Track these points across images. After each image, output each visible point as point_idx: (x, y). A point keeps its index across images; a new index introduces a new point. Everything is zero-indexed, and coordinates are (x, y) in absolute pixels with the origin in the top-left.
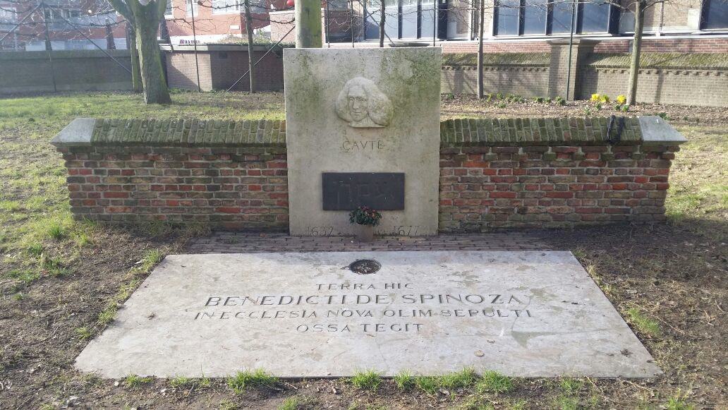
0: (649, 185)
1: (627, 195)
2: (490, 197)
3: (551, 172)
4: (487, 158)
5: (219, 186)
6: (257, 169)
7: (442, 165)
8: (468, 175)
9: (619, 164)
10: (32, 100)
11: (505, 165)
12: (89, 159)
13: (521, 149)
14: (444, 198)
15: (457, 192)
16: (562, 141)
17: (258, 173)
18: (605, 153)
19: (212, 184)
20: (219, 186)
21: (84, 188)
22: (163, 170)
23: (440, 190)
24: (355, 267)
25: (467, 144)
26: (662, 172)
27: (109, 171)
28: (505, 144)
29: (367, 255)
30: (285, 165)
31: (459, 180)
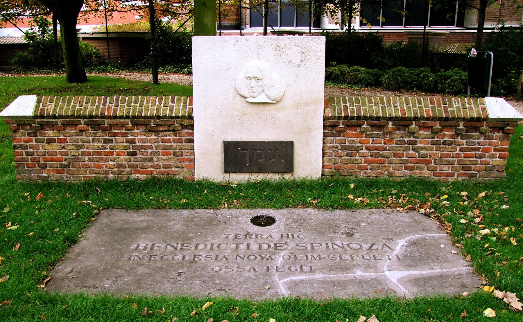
0: (492, 154)
1: (475, 162)
2: (365, 162)
3: (415, 143)
4: (362, 130)
5: (136, 152)
6: (168, 138)
7: (325, 135)
8: (347, 144)
9: (469, 137)
10: (10, 76)
11: (377, 136)
12: (31, 130)
13: (390, 123)
14: (326, 164)
15: (337, 158)
16: (423, 117)
17: (169, 141)
18: (459, 128)
19: (131, 150)
20: (136, 152)
21: (27, 153)
22: (91, 138)
23: (323, 157)
24: (257, 221)
25: (346, 117)
26: (503, 143)
27: (47, 139)
28: (378, 118)
29: (264, 212)
30: (192, 134)
31: (340, 147)
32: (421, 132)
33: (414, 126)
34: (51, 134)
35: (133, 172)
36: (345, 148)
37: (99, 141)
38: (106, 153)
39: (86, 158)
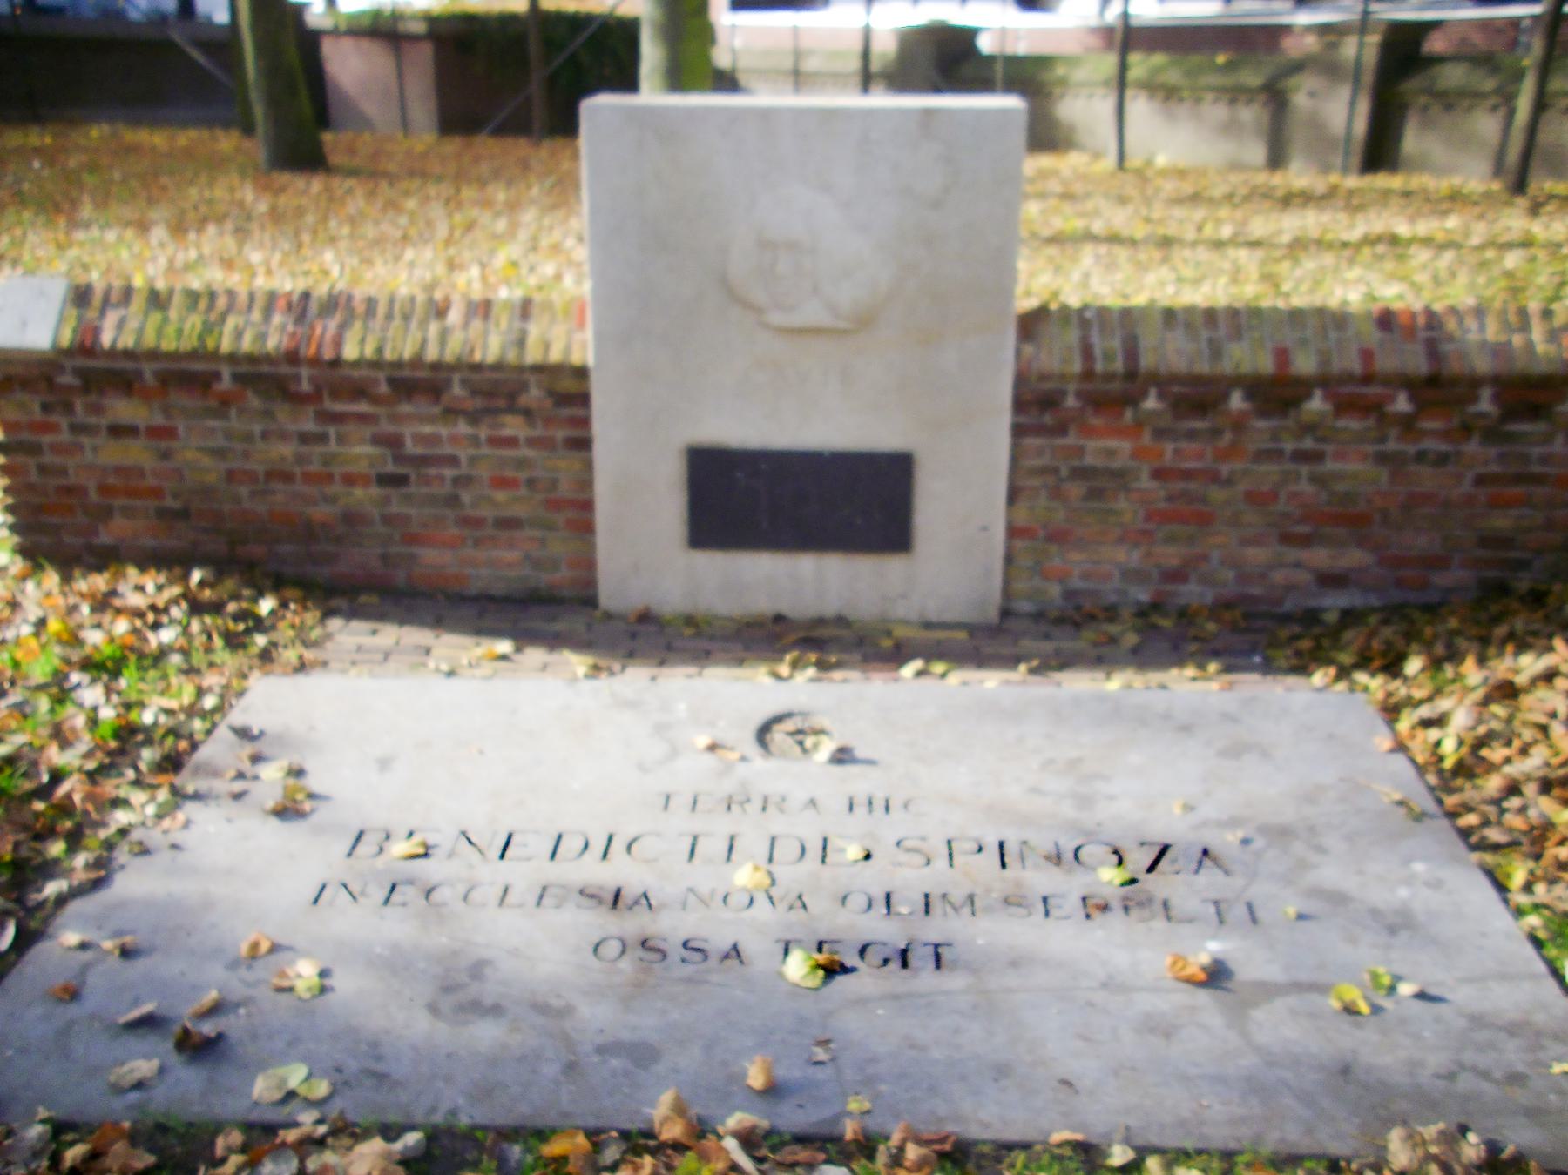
7: (1018, 431)
9: (1510, 438)
11: (1192, 435)
17: (511, 442)
21: (43, 469)
30: (585, 422)
32: (1342, 423)
33: (1316, 404)
34: (124, 410)
35: (397, 537)
36: (1081, 473)
37: (284, 436)
38: (308, 478)
39: (244, 491)
